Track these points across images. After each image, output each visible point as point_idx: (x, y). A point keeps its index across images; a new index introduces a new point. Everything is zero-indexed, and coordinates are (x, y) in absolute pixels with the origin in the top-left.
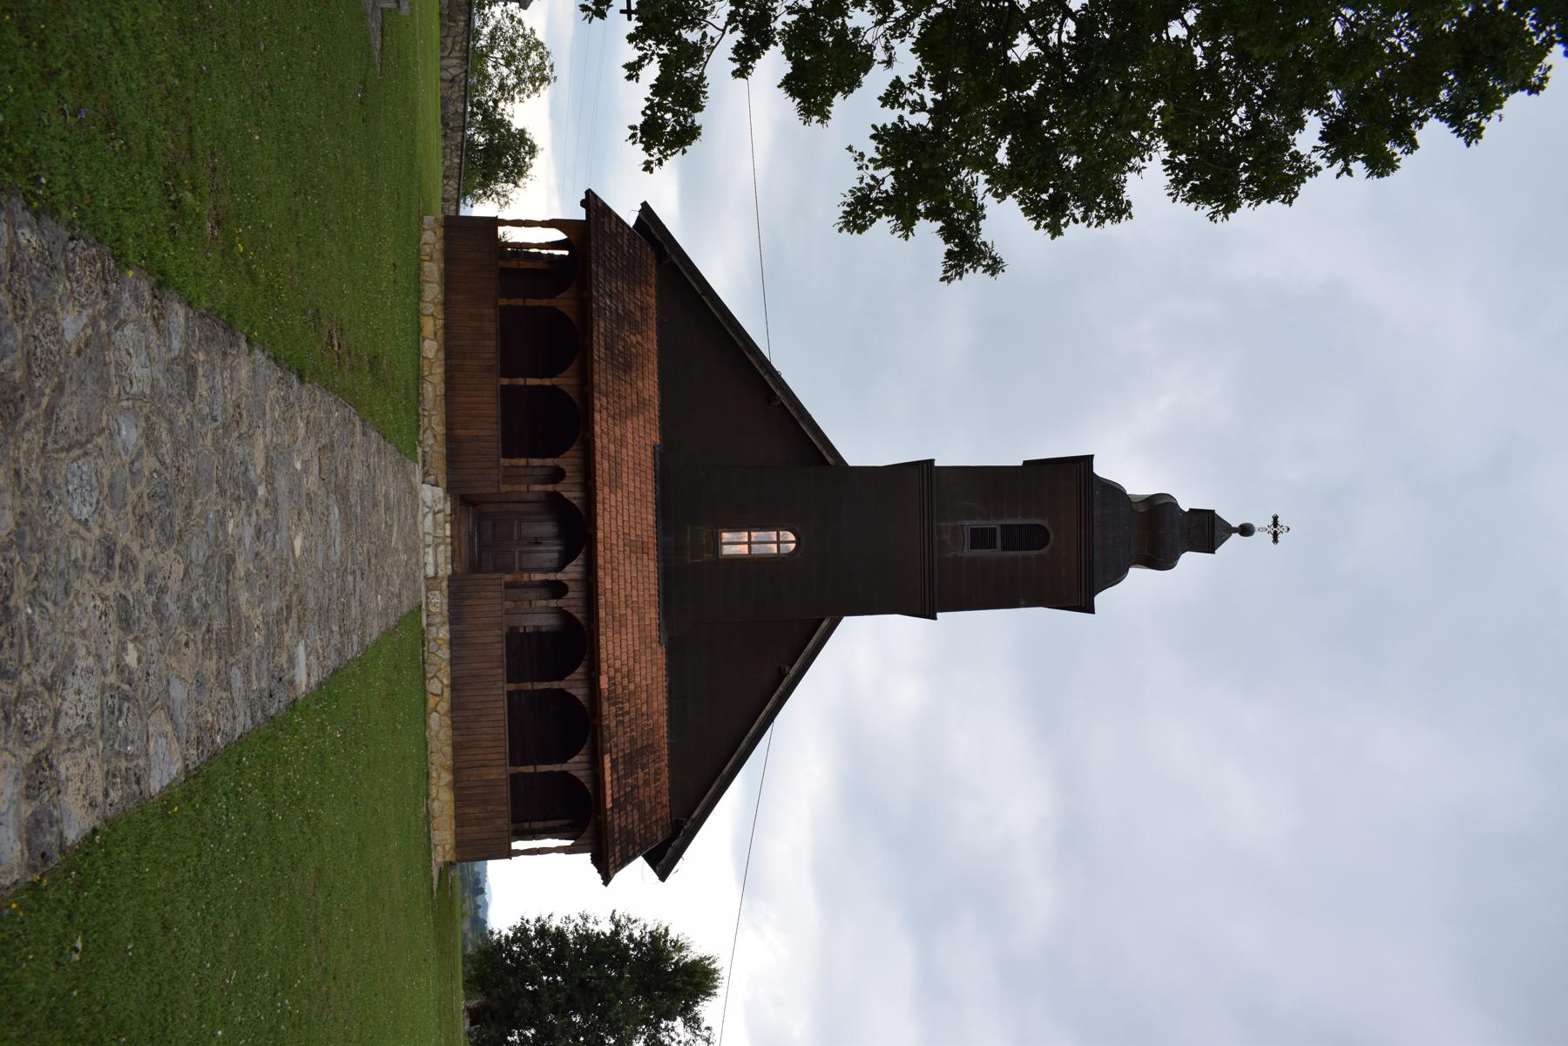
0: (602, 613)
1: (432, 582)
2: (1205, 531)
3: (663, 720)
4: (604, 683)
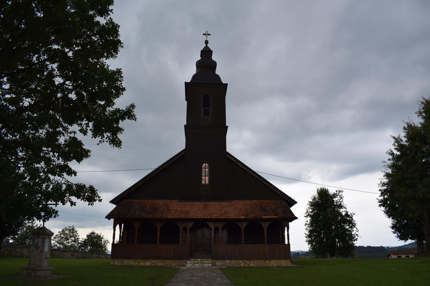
0: (223, 217)
2: (206, 53)
3: (253, 201)
4: (242, 217)
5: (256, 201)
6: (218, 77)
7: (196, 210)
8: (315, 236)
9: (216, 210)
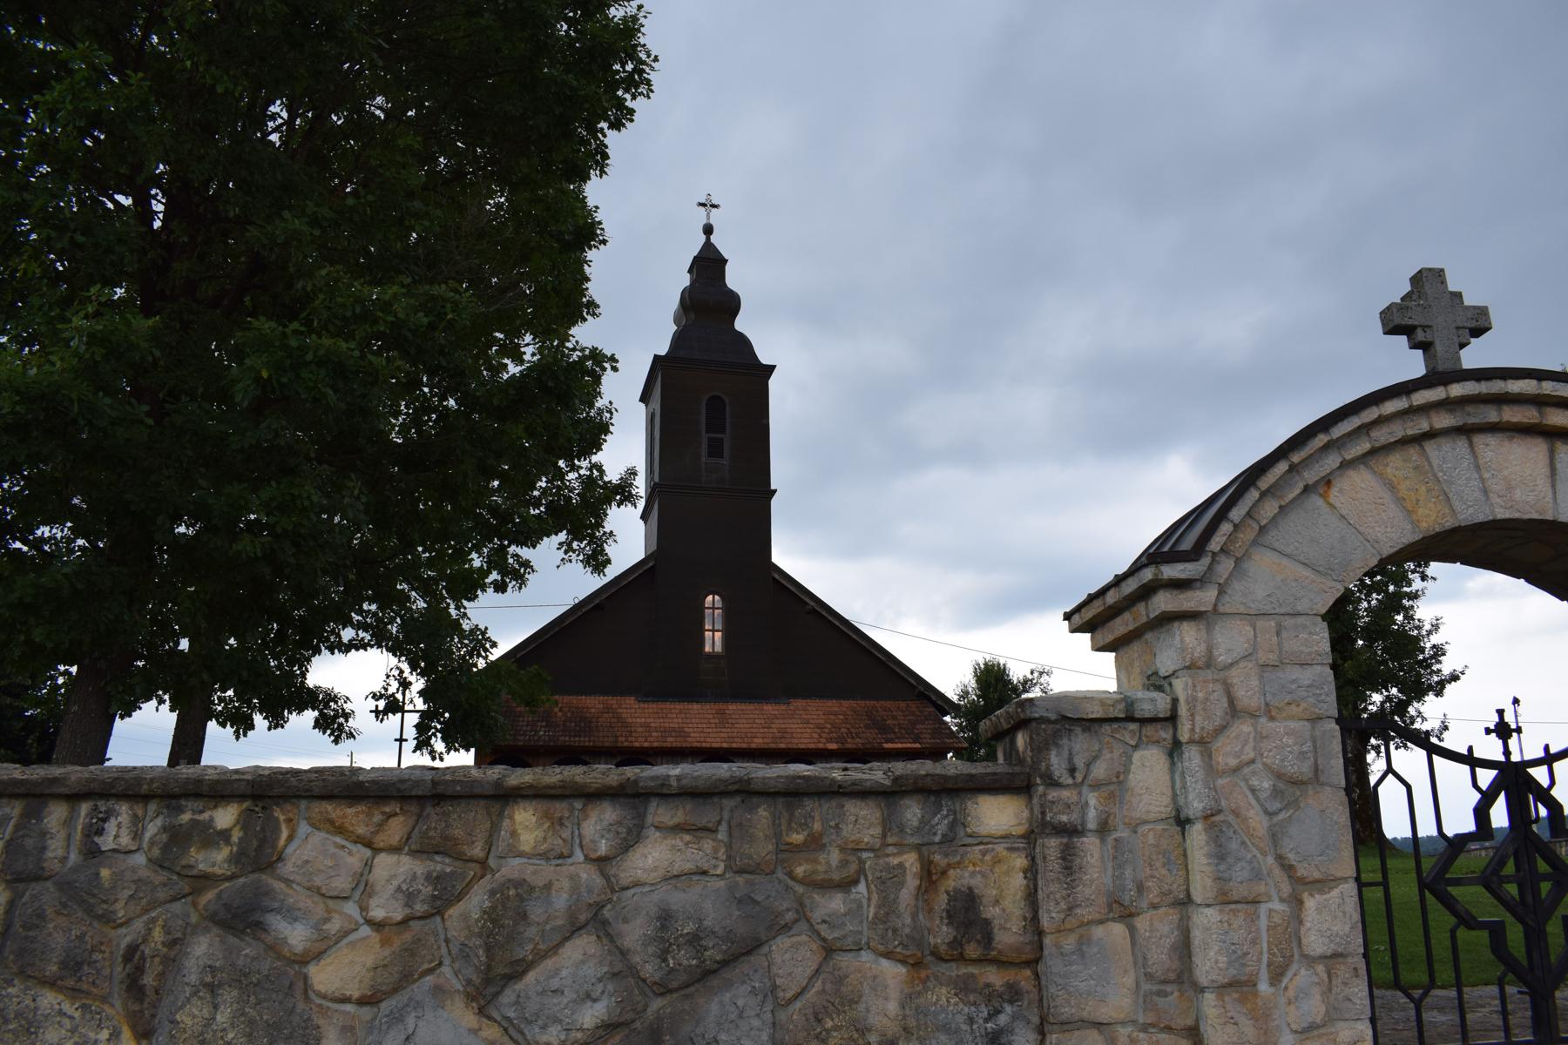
0: (782, 746)
1: (889, 824)
2: (709, 265)
3: (846, 703)
4: (832, 746)
5: (852, 703)
6: (744, 343)
7: (697, 721)
9: (751, 721)
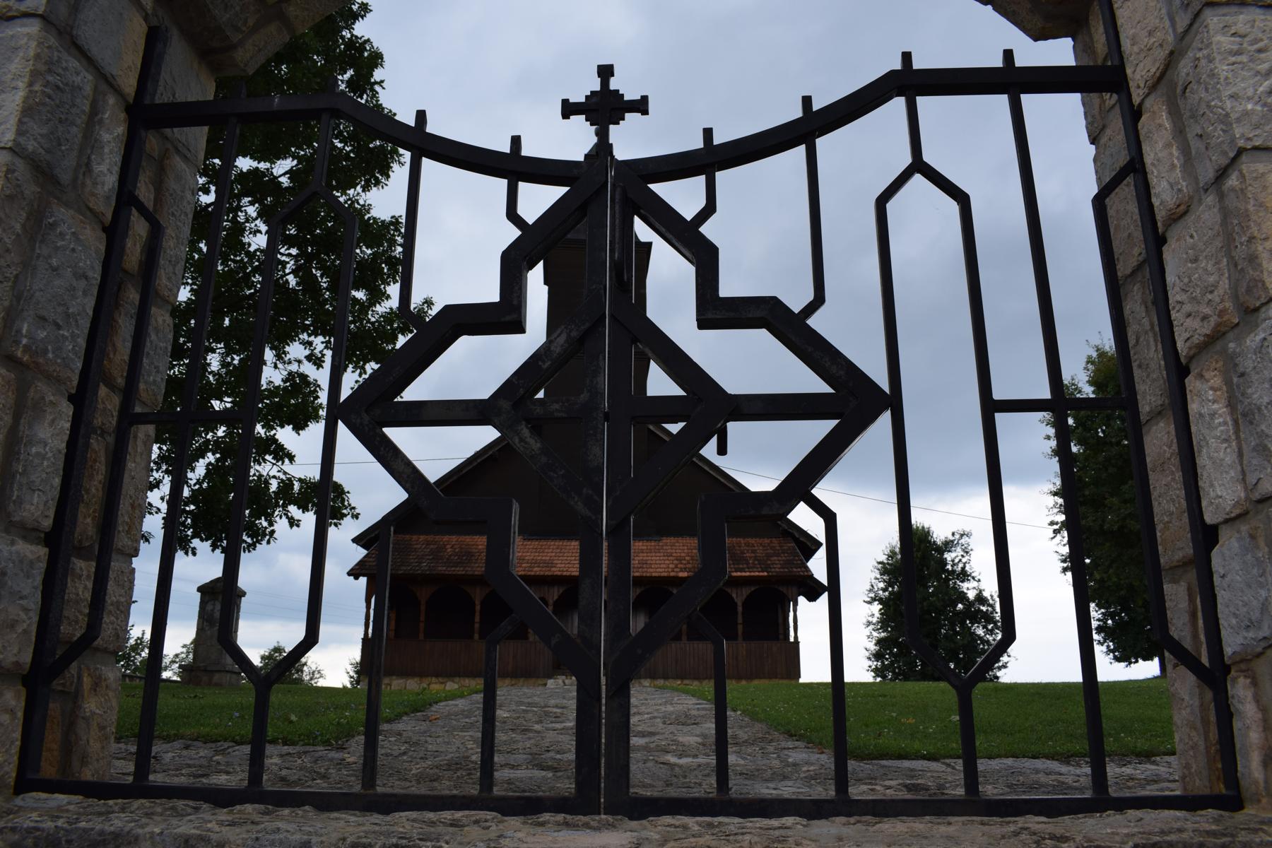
8: (891, 654)
